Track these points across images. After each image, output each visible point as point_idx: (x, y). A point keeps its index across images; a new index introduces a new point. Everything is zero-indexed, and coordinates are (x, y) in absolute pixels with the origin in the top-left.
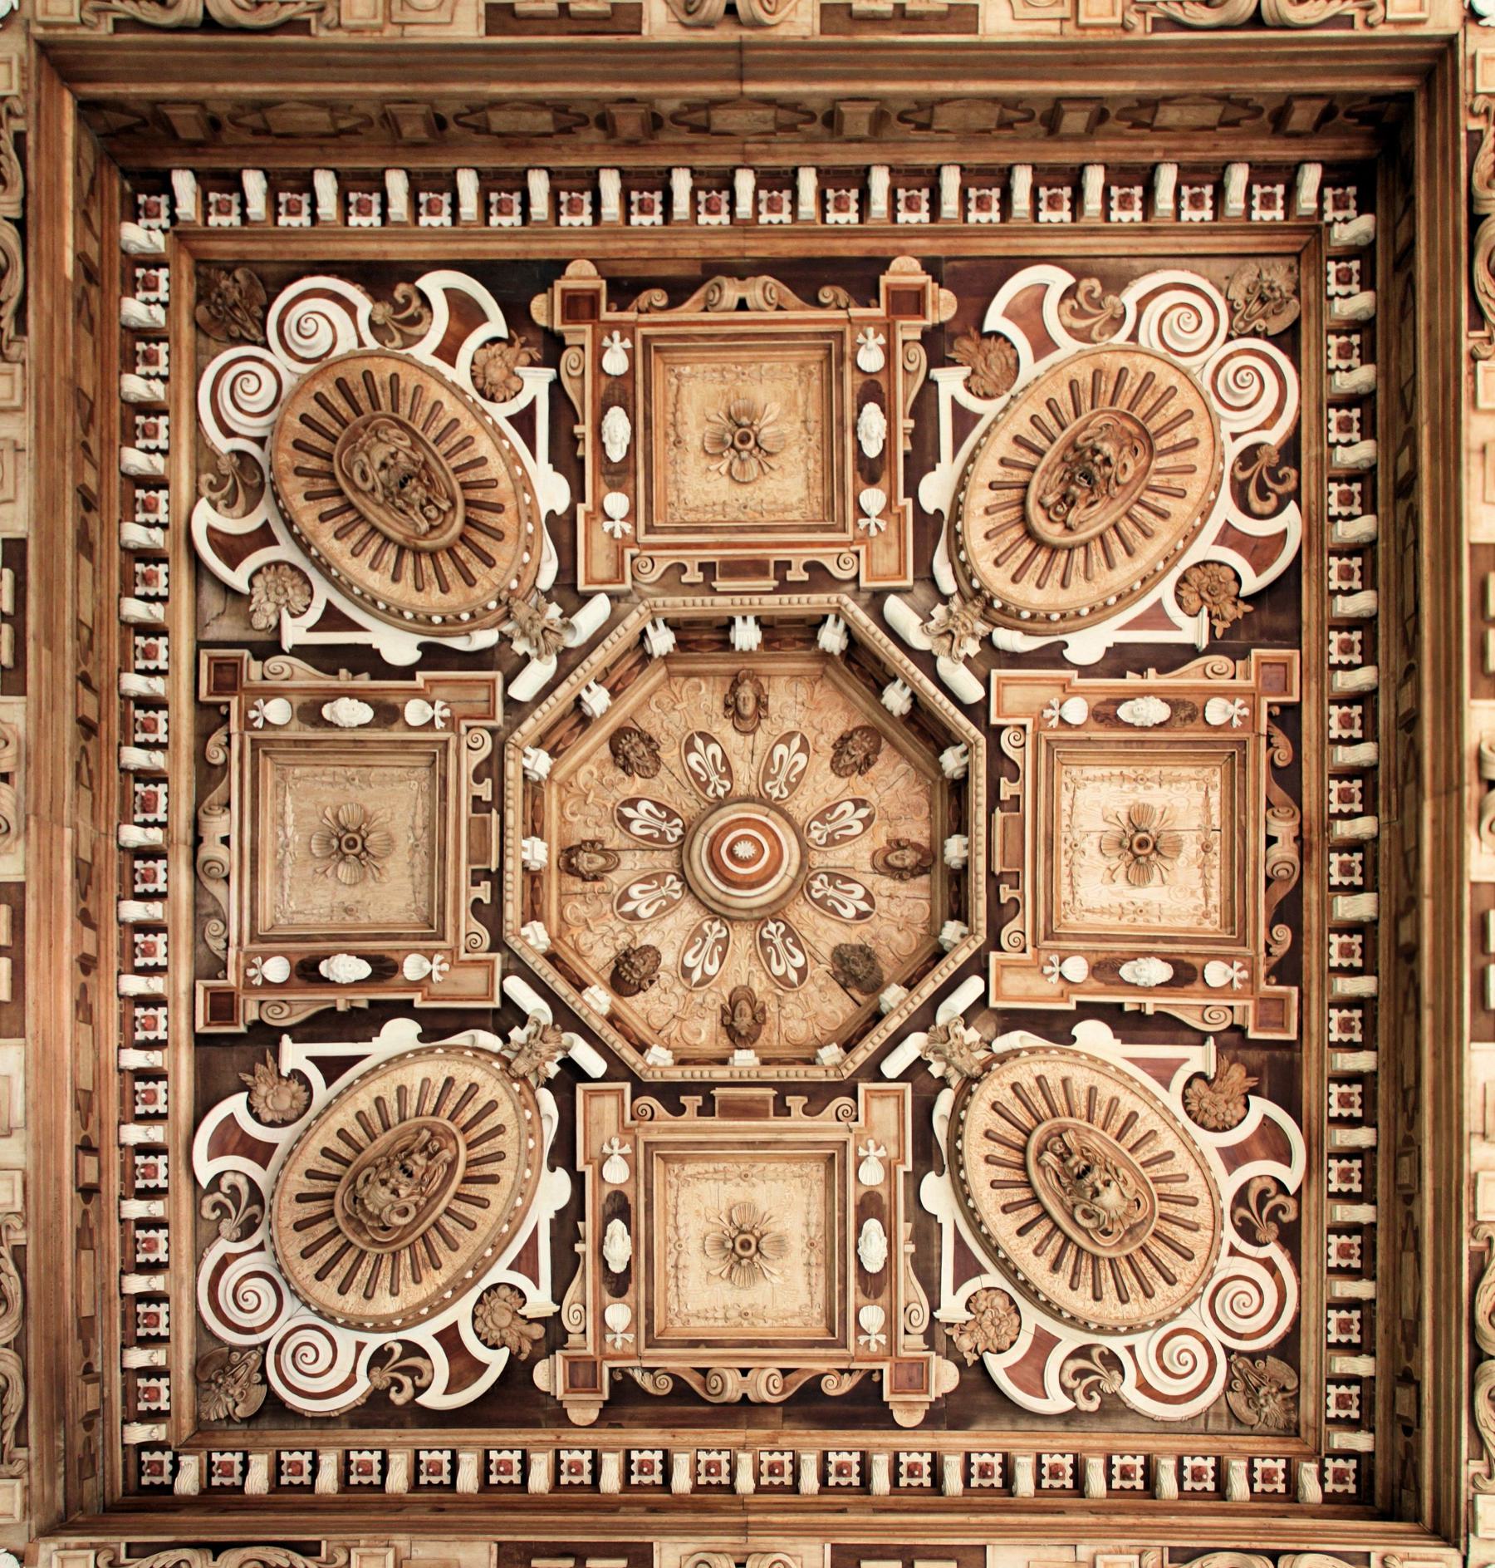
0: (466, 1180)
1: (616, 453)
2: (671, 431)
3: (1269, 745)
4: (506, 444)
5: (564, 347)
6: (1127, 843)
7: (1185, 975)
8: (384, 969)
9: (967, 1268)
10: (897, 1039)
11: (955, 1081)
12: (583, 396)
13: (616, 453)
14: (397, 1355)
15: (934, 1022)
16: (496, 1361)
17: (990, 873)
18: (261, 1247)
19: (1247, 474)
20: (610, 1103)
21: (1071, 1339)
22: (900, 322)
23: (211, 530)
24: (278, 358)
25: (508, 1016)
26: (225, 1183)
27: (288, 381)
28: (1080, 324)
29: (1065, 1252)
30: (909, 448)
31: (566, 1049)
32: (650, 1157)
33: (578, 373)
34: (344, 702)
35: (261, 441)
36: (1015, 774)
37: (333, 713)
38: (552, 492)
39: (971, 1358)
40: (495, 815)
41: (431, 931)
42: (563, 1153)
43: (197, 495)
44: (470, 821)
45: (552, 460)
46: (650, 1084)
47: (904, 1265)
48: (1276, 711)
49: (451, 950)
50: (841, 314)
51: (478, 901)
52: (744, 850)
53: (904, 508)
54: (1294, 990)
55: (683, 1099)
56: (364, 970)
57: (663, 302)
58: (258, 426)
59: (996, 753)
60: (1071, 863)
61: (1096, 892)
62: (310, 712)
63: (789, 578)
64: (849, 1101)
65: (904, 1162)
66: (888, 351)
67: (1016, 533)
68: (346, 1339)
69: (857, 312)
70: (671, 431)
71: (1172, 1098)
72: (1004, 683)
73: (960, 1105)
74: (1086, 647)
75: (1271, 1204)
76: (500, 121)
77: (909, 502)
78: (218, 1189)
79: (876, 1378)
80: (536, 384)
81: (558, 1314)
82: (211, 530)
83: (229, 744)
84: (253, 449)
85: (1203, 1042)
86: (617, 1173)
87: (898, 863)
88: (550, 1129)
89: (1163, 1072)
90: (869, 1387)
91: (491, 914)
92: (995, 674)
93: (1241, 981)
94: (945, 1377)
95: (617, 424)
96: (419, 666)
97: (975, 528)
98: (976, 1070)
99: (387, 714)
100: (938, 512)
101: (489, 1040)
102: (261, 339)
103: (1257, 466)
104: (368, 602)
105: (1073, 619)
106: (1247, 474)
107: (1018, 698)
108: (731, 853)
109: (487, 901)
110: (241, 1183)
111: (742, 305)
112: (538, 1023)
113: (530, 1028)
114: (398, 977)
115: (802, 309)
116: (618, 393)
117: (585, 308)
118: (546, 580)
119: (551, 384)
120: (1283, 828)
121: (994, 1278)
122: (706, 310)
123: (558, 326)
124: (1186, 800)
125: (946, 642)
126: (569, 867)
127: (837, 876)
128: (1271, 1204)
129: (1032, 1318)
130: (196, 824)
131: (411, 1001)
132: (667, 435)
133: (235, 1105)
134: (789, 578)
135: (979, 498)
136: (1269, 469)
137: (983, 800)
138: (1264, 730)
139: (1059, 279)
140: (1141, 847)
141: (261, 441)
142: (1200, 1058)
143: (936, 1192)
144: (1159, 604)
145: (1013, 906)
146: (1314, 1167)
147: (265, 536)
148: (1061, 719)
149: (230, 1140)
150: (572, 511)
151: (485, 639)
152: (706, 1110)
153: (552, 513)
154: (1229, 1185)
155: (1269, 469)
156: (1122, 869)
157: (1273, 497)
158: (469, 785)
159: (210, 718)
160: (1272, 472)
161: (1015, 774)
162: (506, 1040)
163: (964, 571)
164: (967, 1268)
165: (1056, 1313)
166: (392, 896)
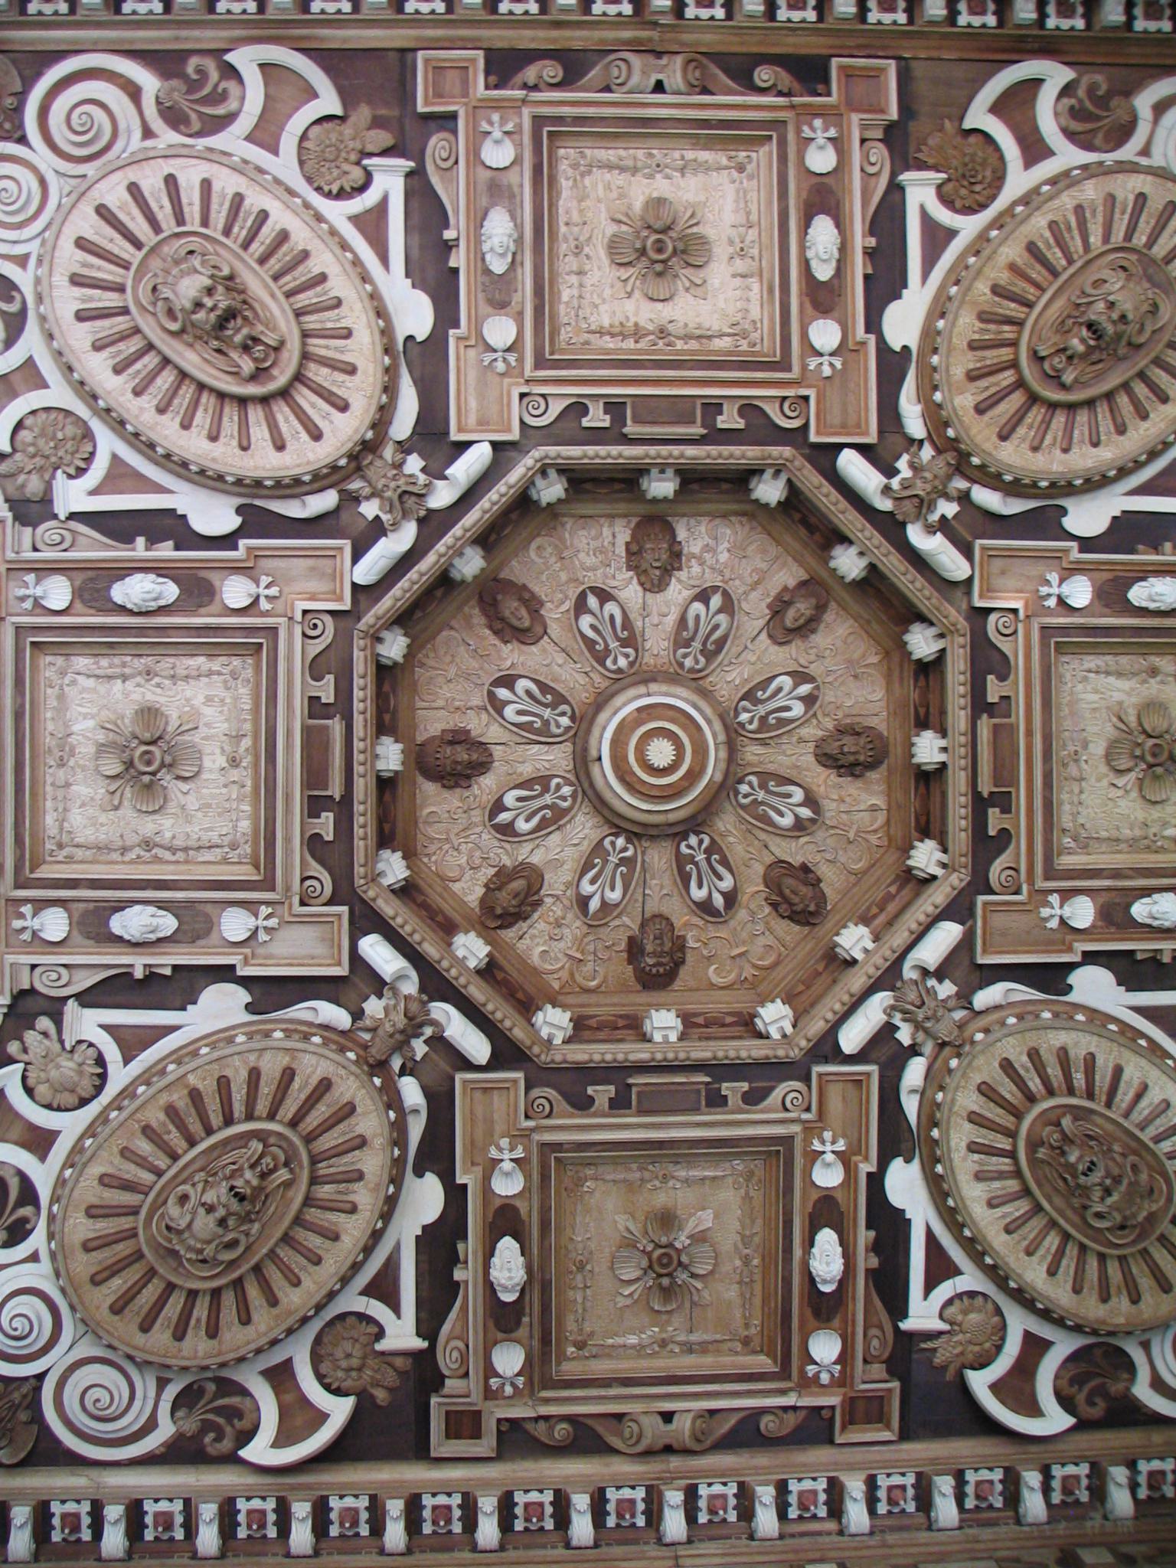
0: (1090, 1095)
1: (168, 923)
2: (132, 855)
3: (535, 88)
4: (68, 1173)
5: (32, 991)
6: (659, 267)
7: (823, 198)
8: (827, 1211)
10: (918, 560)
11: (960, 484)
12: (96, 962)
13: (168, 923)
15: (891, 513)
18: (1146, 1346)
19: (193, 116)
20: (998, 920)
23: (277, 1444)
24: (55, 1360)
26: (231, 85)
27: (84, 1350)
30: (170, 543)
31: (925, 972)
34: (497, 1274)
35: (162, 1383)
38: (221, 1007)
41: (780, 1157)
43: (232, 1459)
44: (641, 1112)
46: (974, 872)
48: (493, 79)
49: (805, 1129)
52: (661, 752)
54: (835, 61)
58: (145, 1386)
59: (550, 434)
60: (687, 337)
61: (721, 303)
62: (504, 1318)
64: (993, 618)
65: (1066, 551)
66: (44, 570)
67: (283, 413)
70: (132, 855)
73: (992, 479)
75: (1088, 104)
78: (222, 78)
81: (55, 517)
82: (277, 1444)
83: (546, 1418)
84: (171, 1392)
87: (524, 612)
88: (1022, 992)
91: (762, 1075)
93: (826, 130)
96: (447, 1177)
97: (264, 461)
98: (950, 457)
99: (505, 1220)
100: (239, 510)
102: (33, 1381)
103: (185, 105)
106: (193, 116)
110: (232, 105)
112: (893, 1008)
113: (897, 1020)
114: (839, 1196)
116: (94, 925)
119: (84, 1005)
120: (639, 71)
124: (603, 192)
128: (1088, 104)
130: (648, 1453)
131: (869, 1174)
133: (980, 1382)
135: (224, 456)
136: (189, 92)
137: (614, 450)
138: (519, 94)
140: (663, 249)
141: (162, 1383)
144: (356, 220)
146: (1050, 47)
147: (281, 1376)
148: (508, 350)
149: (1017, 1388)
150: (246, 982)
151: (411, 1092)
152: (1004, 801)
153: (248, 1007)
155: (189, 92)
156: (688, 271)
157: (223, 85)
158: (595, 1115)
159: (516, 1440)
160: (193, 86)
163: (320, 480)
166: (716, 1212)
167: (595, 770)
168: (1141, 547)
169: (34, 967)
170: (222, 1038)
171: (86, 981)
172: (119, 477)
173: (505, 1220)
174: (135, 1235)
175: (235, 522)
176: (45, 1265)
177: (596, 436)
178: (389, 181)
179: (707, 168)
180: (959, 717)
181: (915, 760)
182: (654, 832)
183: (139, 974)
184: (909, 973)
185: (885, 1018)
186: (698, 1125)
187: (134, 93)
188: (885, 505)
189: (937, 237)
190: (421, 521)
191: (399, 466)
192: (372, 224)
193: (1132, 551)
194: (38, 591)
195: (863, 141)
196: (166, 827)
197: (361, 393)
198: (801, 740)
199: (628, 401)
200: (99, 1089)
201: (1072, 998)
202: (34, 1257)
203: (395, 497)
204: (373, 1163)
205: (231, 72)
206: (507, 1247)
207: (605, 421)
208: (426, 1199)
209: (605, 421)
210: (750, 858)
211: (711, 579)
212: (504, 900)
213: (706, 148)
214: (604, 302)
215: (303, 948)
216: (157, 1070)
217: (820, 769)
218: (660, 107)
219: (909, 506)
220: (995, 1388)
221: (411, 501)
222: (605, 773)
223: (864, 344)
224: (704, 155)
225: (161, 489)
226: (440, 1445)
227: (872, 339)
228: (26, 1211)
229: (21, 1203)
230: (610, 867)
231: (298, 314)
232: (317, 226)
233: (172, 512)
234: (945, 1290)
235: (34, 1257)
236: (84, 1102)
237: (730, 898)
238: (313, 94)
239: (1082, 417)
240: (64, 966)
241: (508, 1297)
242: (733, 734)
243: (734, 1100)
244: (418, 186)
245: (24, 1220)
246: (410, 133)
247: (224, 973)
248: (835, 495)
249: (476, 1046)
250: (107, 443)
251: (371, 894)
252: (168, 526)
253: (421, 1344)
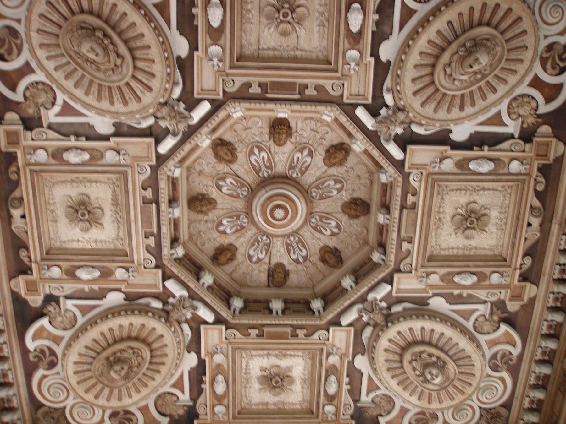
3: (30, 257)
9: (84, 310)
12: (502, 152)
14: (15, 41)
16: (17, 97)
17: (264, 325)
21: (59, 351)
22: (509, 291)
25: (192, 103)
28: (15, 51)
29: (96, 350)
32: (122, 174)
33: (513, 149)
34: (360, 17)
36: (307, 336)
37: (357, 9)
39: (45, 311)
40: (297, 97)
42: (121, 131)
45: (476, 133)
47: (80, 286)
50: (518, 266)
51: (251, 86)
52: (279, 213)
53: (428, 292)
55: (315, 93)
56: (215, 24)
57: (538, 189)
59: (317, 328)
63: (403, 243)
68: (21, 13)
69: (518, 272)
71: (167, 388)
72: (348, 332)
74: (361, 362)
77: (431, 294)
79: (29, 272)
80: (512, 127)
81: (490, 302)
85: (191, 399)
86: (110, 157)
89: (179, 385)
90: (25, 270)
92: (352, 329)
94: (36, 301)
95: (487, 167)
101: (177, 92)
104: (414, 34)
105: (372, 360)
107: (340, 338)
108: (279, 206)
109: (251, 91)
111: (529, 225)
113: (186, 113)
115: (21, 185)
117: (542, 152)
118: (415, 129)
121: (81, 320)
122: (531, 207)
123: (535, 139)
125: (369, 308)
126: (281, 284)
127: (290, 165)
129: (67, 335)
132: (478, 186)
134: (403, 243)
137: (295, 322)
139: (516, 352)
142: (185, 397)
143: (181, 46)
145: (246, 333)
154: (25, 56)
161: (307, 336)
162: (178, 100)
164: (84, 310)
165: (69, 345)
168: (195, 23)
169: (524, 151)
170: (458, 121)
171: (506, 145)
172: (466, 315)
173: (356, 39)
174: (508, 50)
175: (430, 301)
176: (541, 34)
177: (301, 327)
178: (366, 399)
181: (207, 272)
182: (280, 180)
183: (486, 148)
185: (192, 114)
188: (196, 303)
190: (366, 300)
191: (173, 305)
192: (372, 387)
193: (197, 27)
194: (501, 280)
195: (206, 414)
197: (383, 343)
198: (223, 209)
199: (290, 337)
201: (113, 121)
202: (546, 37)
203: (375, 311)
204: (409, 72)
206: (355, 28)
207: (298, 331)
208: (387, 51)
209: (298, 331)
210: (241, 167)
212: (340, 155)
214: (297, 366)
215: (340, 338)
216: (487, 108)
217: (215, 198)
219: (187, 304)
220: (548, 100)
221: (369, 308)
223: (115, 142)
227: (203, 356)
228: (545, 55)
229: (548, 58)
230: (299, 166)
231: (405, 372)
232: (390, 385)
233: (450, 304)
234: (505, 118)
235: (546, 37)
237: (252, 153)
239: (125, 335)
240: (512, 151)
241: (356, 5)
242: (249, 214)
245: (547, 52)
248: (215, 307)
249: (360, 113)
250: (469, 325)
251: (396, 175)
252: (451, 299)
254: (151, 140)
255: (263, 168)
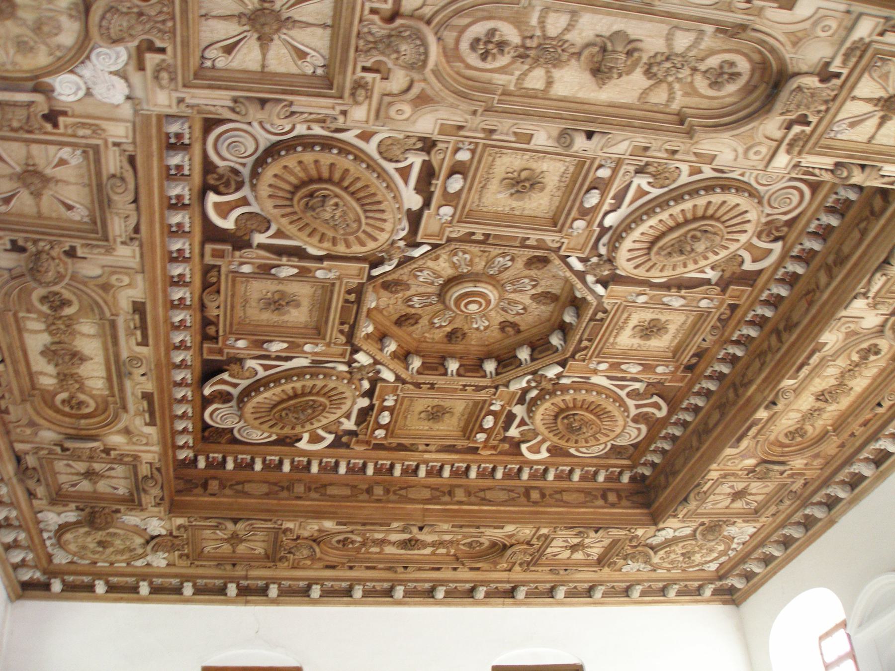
38: (414, 201)
44: (342, 307)
76: (265, 488)
167: (471, 284)
179: (671, 342)
180: (464, 381)
184: (379, 367)
186: (334, 319)
187: (785, 213)
189: (622, 387)
196: (494, 185)
200: (385, 158)
205: (776, 239)
211: (529, 310)
213: (679, 343)
218: (698, 339)
222: (469, 288)
224: (676, 341)
225: (631, 203)
226: (209, 247)
236: (380, 153)
238: (754, 261)
243: (342, 327)
244: (708, 282)
246: (724, 284)
247: (427, 204)
253: (255, 244)
254: (367, 266)
255: (463, 266)
